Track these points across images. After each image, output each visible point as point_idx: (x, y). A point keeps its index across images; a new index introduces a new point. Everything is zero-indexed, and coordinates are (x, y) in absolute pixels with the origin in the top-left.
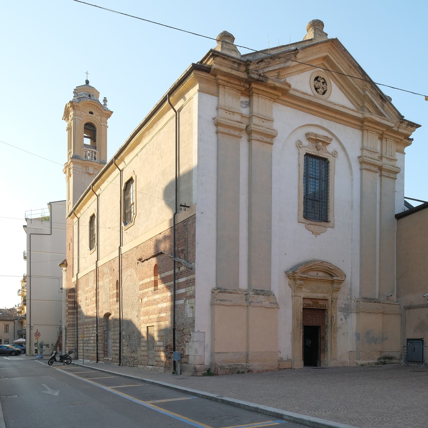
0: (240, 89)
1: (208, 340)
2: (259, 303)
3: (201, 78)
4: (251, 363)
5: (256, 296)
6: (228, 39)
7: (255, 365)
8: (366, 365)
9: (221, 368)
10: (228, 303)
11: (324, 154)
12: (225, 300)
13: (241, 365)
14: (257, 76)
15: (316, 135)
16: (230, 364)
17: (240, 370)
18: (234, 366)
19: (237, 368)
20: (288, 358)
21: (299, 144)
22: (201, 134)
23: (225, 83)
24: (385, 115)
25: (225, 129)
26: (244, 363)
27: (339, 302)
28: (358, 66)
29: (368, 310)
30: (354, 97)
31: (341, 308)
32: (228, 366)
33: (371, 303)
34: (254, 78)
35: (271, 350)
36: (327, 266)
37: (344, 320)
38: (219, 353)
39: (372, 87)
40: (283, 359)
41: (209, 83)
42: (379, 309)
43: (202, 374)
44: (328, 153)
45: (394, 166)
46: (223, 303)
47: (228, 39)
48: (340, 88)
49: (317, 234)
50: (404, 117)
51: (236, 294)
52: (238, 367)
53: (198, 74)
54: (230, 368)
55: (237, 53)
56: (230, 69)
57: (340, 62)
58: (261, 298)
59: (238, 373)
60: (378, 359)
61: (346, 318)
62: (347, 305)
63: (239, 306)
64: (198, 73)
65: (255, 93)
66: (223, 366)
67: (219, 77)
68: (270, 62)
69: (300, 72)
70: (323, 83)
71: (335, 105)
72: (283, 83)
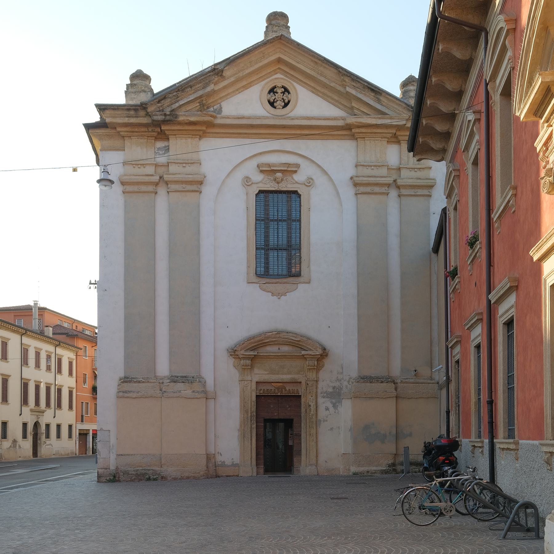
0: (150, 135)
1: (113, 440)
2: (176, 392)
3: (101, 136)
4: (165, 468)
5: (172, 384)
6: (137, 80)
7: (170, 471)
8: (364, 474)
9: (124, 473)
10: (135, 395)
11: (289, 186)
12: (130, 392)
13: (152, 469)
14: (161, 116)
15: (269, 165)
16: (137, 468)
17: (151, 476)
18: (142, 471)
19: (146, 474)
20: (233, 462)
21: (246, 182)
22: (104, 199)
23: (129, 134)
24: (386, 111)
25: (133, 187)
26: (159, 467)
27: (321, 384)
28: (323, 59)
29: (366, 394)
30: (336, 98)
31: (326, 392)
32: (135, 471)
33: (373, 384)
34: (158, 120)
35: (194, 451)
36: (289, 338)
37: (332, 409)
38: (122, 455)
39: (353, 80)
40: (225, 463)
41: (112, 138)
42: (388, 391)
43: (106, 479)
44: (297, 183)
45: (420, 179)
46: (126, 395)
47: (138, 79)
48: (313, 92)
49: (280, 295)
50: (125, 91)
51: (147, 383)
52: (148, 472)
53: (95, 133)
54: (137, 474)
55: (147, 93)
56: (127, 117)
57: (300, 60)
58: (180, 386)
59: (149, 479)
60: (387, 466)
61: (335, 406)
62: (337, 388)
63: (149, 397)
64: (95, 132)
65: (170, 135)
66: (127, 470)
67: (119, 129)
68: (177, 95)
69: (242, 89)
70: (283, 93)
71: (293, 119)
72: (201, 115)
